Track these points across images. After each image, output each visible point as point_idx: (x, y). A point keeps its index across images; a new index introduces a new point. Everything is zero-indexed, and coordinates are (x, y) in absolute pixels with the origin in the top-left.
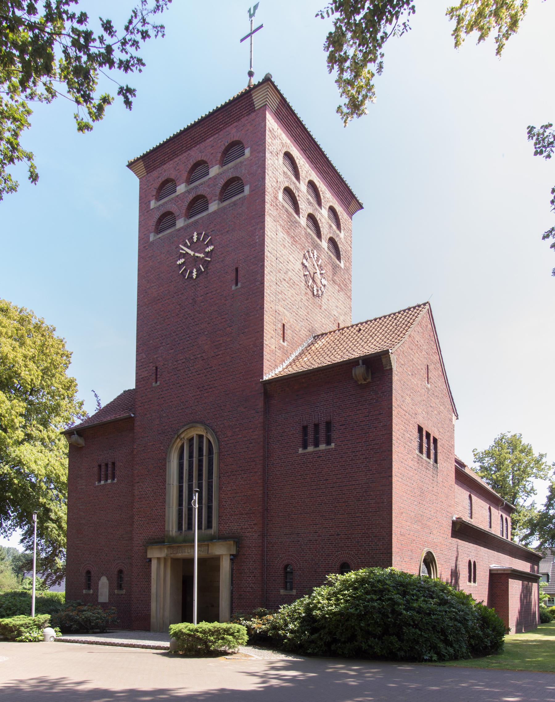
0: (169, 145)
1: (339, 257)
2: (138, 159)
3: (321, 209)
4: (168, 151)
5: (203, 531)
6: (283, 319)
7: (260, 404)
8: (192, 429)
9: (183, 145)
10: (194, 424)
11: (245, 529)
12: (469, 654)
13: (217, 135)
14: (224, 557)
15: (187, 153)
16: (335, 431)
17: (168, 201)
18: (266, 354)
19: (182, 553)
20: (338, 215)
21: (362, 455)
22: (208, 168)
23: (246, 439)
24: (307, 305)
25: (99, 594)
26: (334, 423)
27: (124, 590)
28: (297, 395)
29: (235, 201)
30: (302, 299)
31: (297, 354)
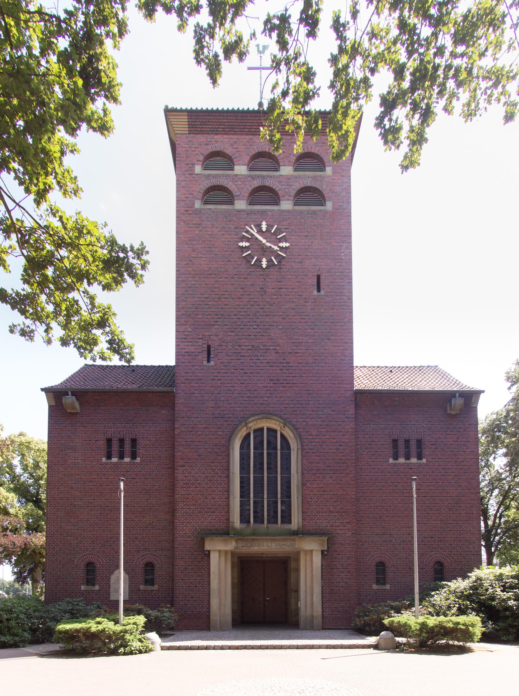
0: (228, 116)
4: (225, 122)
5: (279, 526)
7: (352, 411)
8: (264, 420)
9: (246, 125)
10: (269, 416)
11: (336, 526)
12: (36, 638)
14: (314, 552)
17: (221, 175)
19: (260, 546)
21: (453, 472)
23: (335, 440)
25: (112, 590)
27: (157, 586)
28: (386, 411)
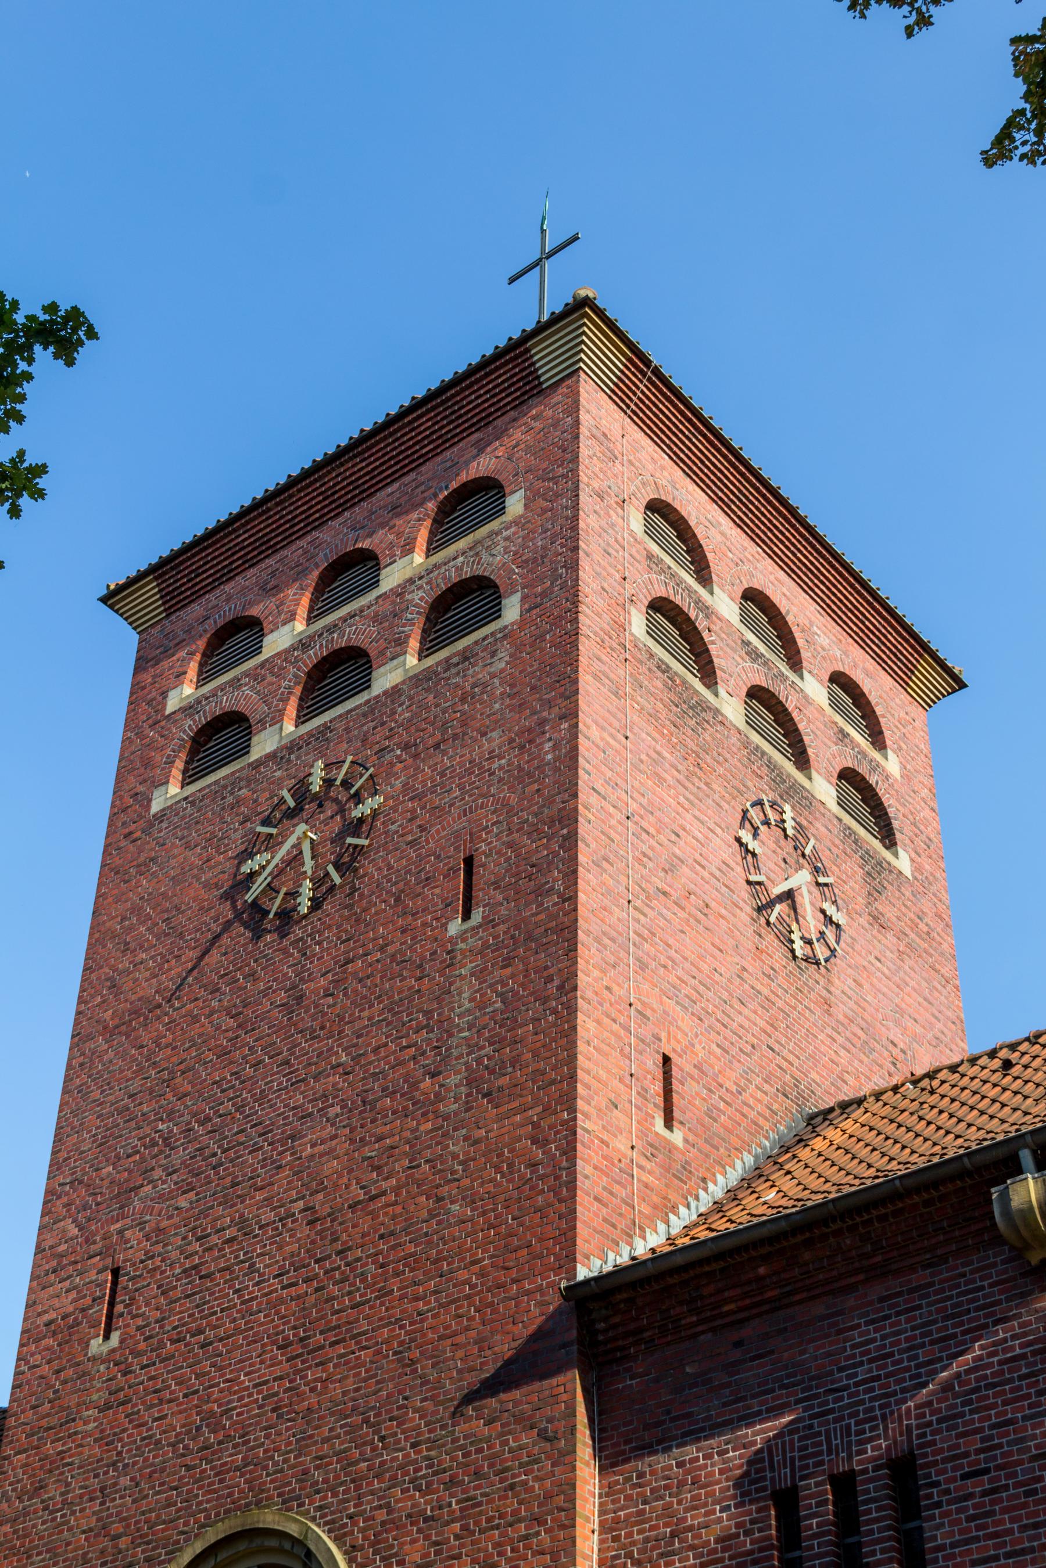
1: (888, 836)
2: (141, 576)
3: (802, 677)
6: (663, 1035)
13: (413, 475)
15: (309, 538)
16: (938, 1505)
18: (588, 1170)
20: (869, 703)
22: (377, 568)
24: (766, 992)
26: (928, 1465)
28: (738, 1344)
29: (466, 649)
30: (744, 969)
31: (733, 1182)
